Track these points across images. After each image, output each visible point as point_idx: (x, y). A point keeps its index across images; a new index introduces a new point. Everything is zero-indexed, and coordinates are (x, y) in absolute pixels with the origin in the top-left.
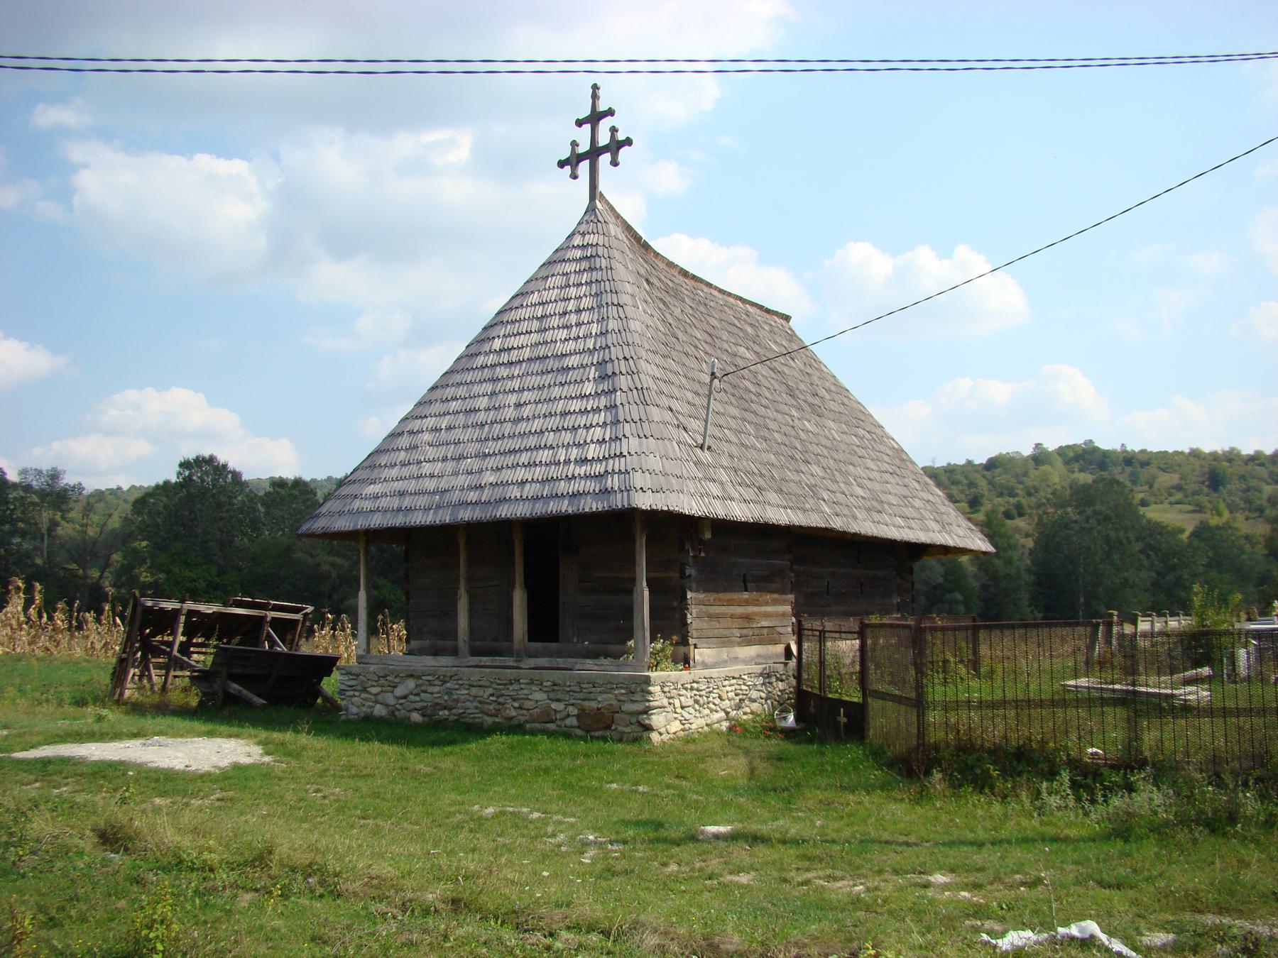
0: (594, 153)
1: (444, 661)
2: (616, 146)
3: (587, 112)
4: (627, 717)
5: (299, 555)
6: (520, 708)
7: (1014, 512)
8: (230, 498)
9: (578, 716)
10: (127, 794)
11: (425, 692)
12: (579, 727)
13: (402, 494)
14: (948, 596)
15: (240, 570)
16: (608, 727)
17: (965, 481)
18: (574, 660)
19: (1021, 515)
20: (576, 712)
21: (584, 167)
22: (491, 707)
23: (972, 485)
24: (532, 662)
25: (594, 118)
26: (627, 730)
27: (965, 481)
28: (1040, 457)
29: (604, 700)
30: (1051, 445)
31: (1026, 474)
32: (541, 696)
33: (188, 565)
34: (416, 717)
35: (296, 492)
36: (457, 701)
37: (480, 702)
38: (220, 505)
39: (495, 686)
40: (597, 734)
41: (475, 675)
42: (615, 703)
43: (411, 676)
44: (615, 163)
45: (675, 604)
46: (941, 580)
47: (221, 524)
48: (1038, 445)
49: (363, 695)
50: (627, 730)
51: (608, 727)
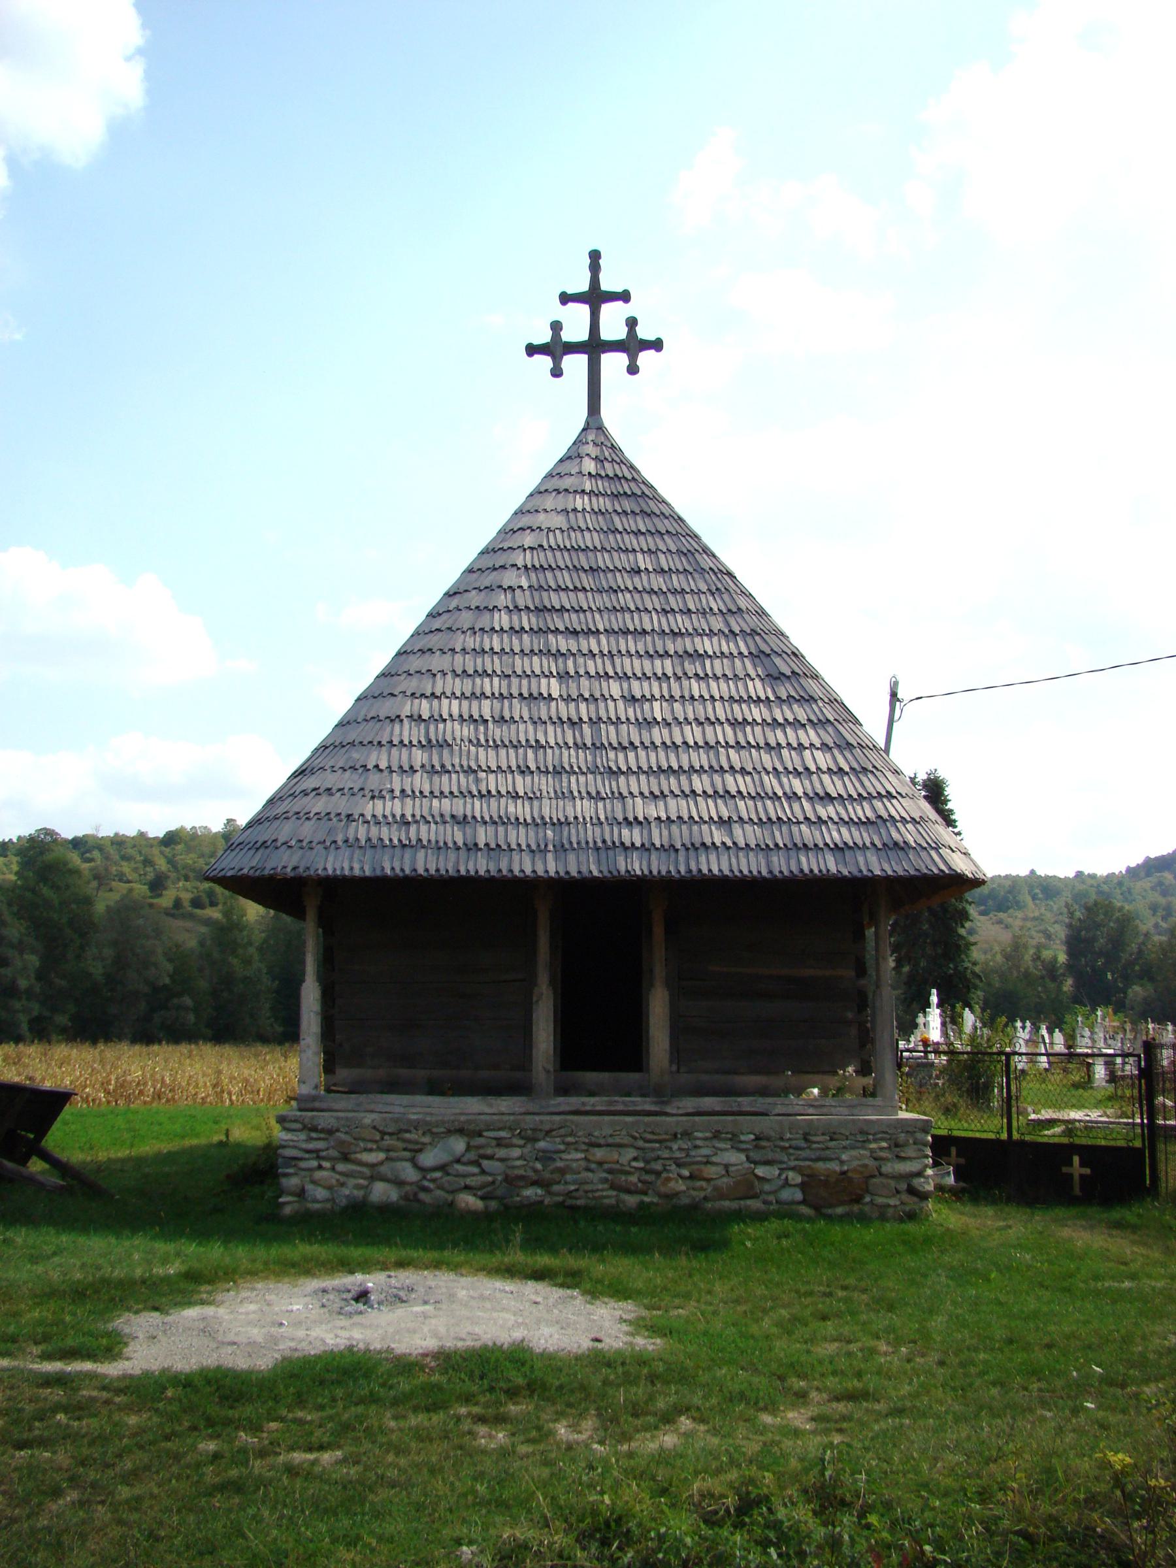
0: (594, 347)
1: (506, 1104)
2: (633, 345)
3: (583, 286)
4: (892, 1183)
6: (692, 1177)
7: (206, 901)
9: (803, 1186)
11: (490, 1157)
12: (804, 1202)
13: (462, 821)
14: (175, 1001)
16: (858, 1200)
17: (139, 858)
18: (770, 1100)
19: (213, 904)
20: (799, 1179)
21: (577, 364)
22: (634, 1179)
23: (147, 862)
24: (690, 1104)
25: (595, 297)
26: (893, 1202)
27: (139, 858)
29: (851, 1159)
32: (735, 1158)
34: (469, 1201)
36: (563, 1171)
37: (610, 1171)
39: (640, 1143)
40: (840, 1210)
41: (605, 1127)
42: (872, 1163)
43: (461, 1131)
44: (633, 370)
45: (850, 1015)
46: (167, 981)
48: (229, 821)
49: (341, 1167)
50: (893, 1202)
51: (858, 1200)
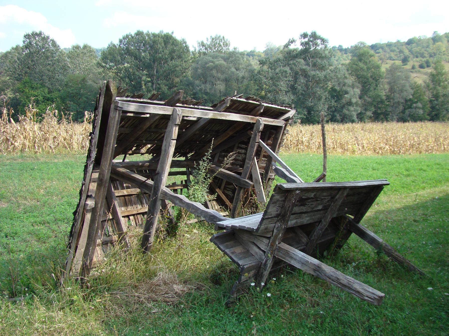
5: (90, 82)
7: (425, 65)
8: (52, 54)
10: (138, 306)
14: (414, 105)
15: (59, 91)
17: (397, 50)
19: (428, 66)
27: (397, 50)
28: (436, 39)
30: (441, 33)
31: (428, 47)
33: (33, 88)
35: (85, 51)
38: (47, 58)
47: (48, 67)
